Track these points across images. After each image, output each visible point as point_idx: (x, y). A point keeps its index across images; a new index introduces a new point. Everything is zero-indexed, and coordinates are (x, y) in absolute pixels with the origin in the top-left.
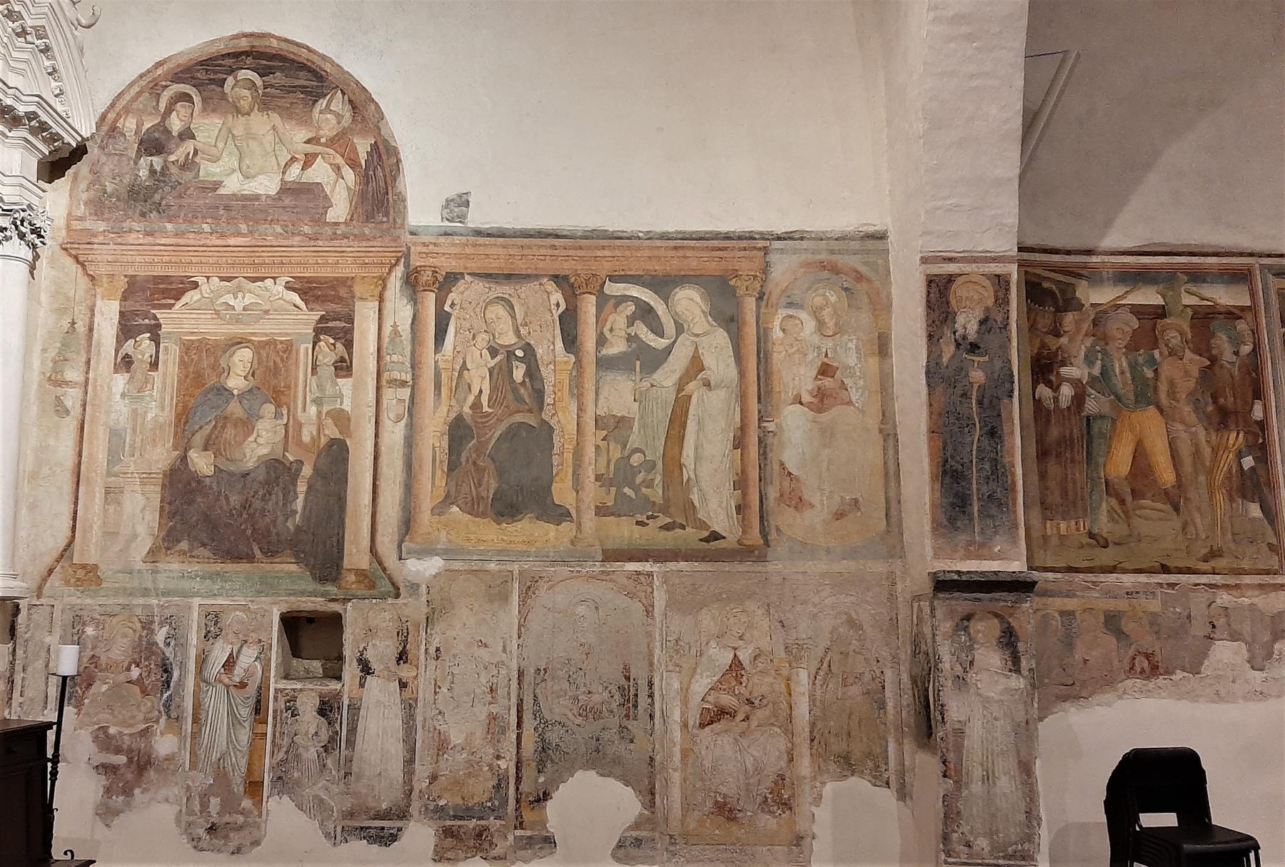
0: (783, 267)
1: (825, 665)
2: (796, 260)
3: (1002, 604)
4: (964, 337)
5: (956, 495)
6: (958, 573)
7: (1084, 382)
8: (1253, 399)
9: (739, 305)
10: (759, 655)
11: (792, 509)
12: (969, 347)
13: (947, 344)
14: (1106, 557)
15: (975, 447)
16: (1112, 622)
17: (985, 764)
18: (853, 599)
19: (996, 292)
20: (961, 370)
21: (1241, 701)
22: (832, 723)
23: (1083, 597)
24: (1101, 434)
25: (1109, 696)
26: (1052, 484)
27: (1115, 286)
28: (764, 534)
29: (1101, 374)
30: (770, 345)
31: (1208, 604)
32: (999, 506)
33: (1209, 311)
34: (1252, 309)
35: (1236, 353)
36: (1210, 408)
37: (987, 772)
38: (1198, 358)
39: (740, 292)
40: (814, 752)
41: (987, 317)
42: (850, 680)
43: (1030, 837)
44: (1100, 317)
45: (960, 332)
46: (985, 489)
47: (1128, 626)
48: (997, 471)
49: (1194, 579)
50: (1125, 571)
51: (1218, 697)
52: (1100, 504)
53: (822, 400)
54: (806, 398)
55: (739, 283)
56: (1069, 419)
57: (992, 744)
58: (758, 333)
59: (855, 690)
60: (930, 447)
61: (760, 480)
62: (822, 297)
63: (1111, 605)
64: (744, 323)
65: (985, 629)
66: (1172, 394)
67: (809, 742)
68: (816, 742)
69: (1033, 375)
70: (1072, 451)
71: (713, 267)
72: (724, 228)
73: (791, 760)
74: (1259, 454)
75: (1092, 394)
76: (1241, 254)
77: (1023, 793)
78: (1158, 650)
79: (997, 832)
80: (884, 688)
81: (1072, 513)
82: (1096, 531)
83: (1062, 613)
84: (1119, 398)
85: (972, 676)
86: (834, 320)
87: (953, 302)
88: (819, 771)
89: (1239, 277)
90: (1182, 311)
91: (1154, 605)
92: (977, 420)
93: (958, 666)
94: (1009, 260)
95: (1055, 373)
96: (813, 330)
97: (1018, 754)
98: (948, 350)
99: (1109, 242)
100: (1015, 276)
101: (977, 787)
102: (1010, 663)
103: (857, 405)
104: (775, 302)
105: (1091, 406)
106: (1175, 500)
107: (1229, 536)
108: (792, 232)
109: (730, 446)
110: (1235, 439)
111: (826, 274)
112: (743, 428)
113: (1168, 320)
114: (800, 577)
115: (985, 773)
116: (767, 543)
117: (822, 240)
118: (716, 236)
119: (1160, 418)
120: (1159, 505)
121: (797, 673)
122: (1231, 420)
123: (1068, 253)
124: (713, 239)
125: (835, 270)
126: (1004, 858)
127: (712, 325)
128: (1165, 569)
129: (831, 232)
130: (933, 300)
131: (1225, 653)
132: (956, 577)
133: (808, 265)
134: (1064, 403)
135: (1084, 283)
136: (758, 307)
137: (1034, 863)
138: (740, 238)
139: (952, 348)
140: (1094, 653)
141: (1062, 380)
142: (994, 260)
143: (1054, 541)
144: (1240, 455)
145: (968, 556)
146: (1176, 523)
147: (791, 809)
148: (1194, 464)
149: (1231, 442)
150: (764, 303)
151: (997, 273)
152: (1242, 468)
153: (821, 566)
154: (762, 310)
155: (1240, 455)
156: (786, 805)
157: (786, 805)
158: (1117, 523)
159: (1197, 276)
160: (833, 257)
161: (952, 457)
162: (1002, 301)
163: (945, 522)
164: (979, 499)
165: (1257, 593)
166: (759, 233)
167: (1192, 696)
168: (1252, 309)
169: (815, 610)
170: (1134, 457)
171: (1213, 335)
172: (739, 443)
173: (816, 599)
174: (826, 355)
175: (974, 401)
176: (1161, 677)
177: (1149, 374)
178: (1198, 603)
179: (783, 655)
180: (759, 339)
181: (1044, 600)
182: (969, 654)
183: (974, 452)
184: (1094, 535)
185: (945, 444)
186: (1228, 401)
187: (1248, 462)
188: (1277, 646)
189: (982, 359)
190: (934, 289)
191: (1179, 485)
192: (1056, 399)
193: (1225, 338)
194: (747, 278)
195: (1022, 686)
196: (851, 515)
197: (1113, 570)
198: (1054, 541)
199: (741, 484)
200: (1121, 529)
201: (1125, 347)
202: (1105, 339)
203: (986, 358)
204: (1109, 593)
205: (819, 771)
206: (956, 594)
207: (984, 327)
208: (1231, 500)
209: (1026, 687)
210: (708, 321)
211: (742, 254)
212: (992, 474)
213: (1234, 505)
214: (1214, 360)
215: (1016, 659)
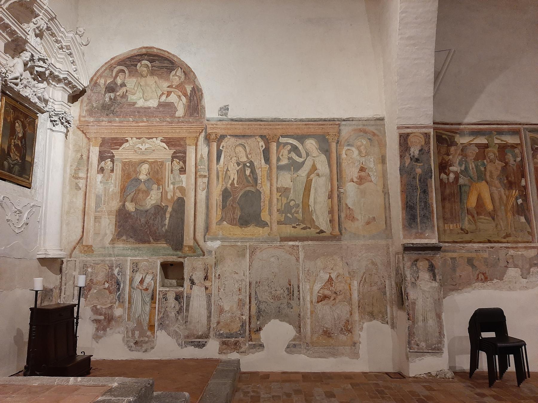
0: (346, 131)
1: (363, 279)
3: (429, 255)
4: (414, 156)
5: (412, 215)
6: (413, 244)
9: (329, 145)
14: (467, 237)
15: (418, 197)
16: (470, 261)
18: (374, 254)
19: (425, 139)
20: (413, 169)
21: (519, 290)
22: (366, 300)
24: (465, 191)
28: (340, 230)
29: (465, 169)
30: (341, 160)
33: (504, 145)
34: (521, 144)
35: (515, 161)
36: (505, 181)
38: (501, 163)
39: (330, 141)
40: (360, 311)
43: (440, 342)
44: (464, 148)
45: (412, 154)
47: (476, 263)
48: (427, 206)
50: (474, 243)
51: (510, 289)
53: (361, 180)
54: (355, 180)
55: (329, 137)
56: (453, 186)
58: (337, 156)
59: (375, 288)
61: (338, 210)
63: (470, 255)
65: (423, 265)
66: (491, 176)
68: (360, 307)
71: (320, 131)
72: (324, 117)
73: (351, 314)
76: (516, 124)
79: (428, 340)
81: (455, 221)
82: (463, 228)
83: (451, 258)
84: (471, 178)
85: (418, 282)
87: (409, 143)
89: (515, 132)
91: (486, 255)
93: (413, 278)
94: (430, 127)
98: (408, 161)
99: (466, 120)
100: (432, 133)
101: (420, 324)
102: (432, 277)
103: (374, 182)
105: (461, 181)
106: (493, 216)
107: (513, 229)
108: (349, 118)
109: (327, 198)
110: (515, 193)
111: (362, 133)
112: (332, 191)
113: (489, 149)
116: (341, 234)
118: (321, 120)
120: (487, 218)
123: (452, 124)
125: (365, 132)
127: (320, 153)
128: (490, 242)
129: (363, 118)
131: (513, 272)
133: (355, 130)
134: (451, 180)
135: (458, 135)
136: (337, 146)
138: (329, 121)
139: (409, 160)
142: (424, 127)
143: (448, 232)
144: (517, 199)
145: (416, 238)
146: (494, 224)
147: (351, 332)
149: (513, 194)
155: (517, 199)
156: (350, 331)
157: (350, 331)
158: (471, 224)
159: (500, 132)
160: (365, 127)
162: (427, 143)
163: (407, 225)
164: (420, 216)
165: (524, 250)
166: (336, 119)
167: (500, 288)
169: (359, 259)
172: (330, 197)
173: (360, 255)
175: (417, 180)
177: (483, 169)
178: (502, 254)
179: (348, 275)
183: (418, 199)
186: (512, 179)
187: (520, 201)
188: (532, 269)
189: (420, 164)
191: (494, 210)
192: (448, 179)
193: (510, 155)
194: (332, 135)
195: (437, 286)
197: (470, 242)
198: (448, 232)
199: (331, 212)
202: (466, 156)
204: (468, 251)
205: (362, 318)
206: (412, 252)
207: (421, 152)
208: (514, 215)
209: (438, 286)
211: (331, 126)
214: (507, 163)
215: (434, 276)
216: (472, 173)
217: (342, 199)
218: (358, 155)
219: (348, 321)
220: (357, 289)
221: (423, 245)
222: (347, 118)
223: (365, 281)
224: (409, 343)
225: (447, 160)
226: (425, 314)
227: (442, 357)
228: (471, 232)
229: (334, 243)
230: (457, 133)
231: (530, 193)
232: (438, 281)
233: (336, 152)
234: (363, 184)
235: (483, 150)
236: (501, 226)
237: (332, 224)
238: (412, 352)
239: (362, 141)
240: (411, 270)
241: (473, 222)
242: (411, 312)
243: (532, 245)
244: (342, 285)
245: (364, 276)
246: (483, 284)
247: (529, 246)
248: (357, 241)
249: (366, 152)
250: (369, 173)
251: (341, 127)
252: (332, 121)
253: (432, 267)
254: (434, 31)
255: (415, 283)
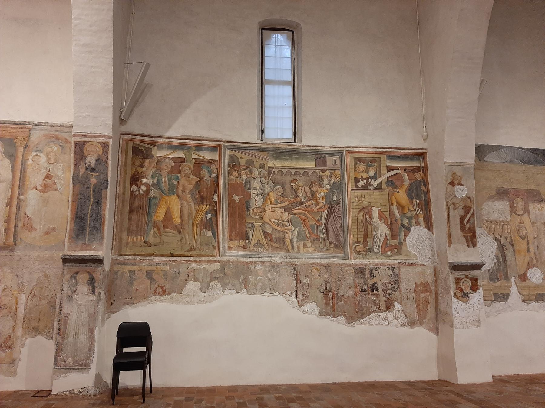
0: (36, 136)
1: (33, 292)
2: (42, 133)
3: (90, 268)
4: (89, 166)
5: (80, 226)
6: (70, 256)
7: (150, 185)
8: (214, 193)
9: (16, 151)
10: (6, 288)
11: (28, 231)
12: (91, 169)
13: (82, 168)
14: (150, 250)
15: (90, 207)
16: (149, 275)
17: (75, 329)
18: (48, 266)
19: (103, 149)
20: (87, 178)
21: (196, 304)
22: (33, 315)
23: (139, 265)
24: (154, 204)
25: (146, 303)
26: (133, 223)
27: (167, 150)
28: (15, 240)
29: (157, 182)
30: (26, 166)
31: (187, 268)
32: (97, 230)
33: (201, 161)
34: (218, 161)
35: (210, 177)
36: (197, 196)
37: (76, 333)
38: (195, 177)
39: (17, 145)
40: (24, 326)
41: (99, 158)
42: (43, 298)
43: (89, 358)
44: (160, 161)
45: (88, 163)
46: (92, 224)
47: (155, 276)
48: (99, 218)
49: (183, 258)
50: (156, 256)
51: (187, 303)
52: (151, 230)
53: (45, 188)
54: (39, 187)
55: (17, 141)
56: (143, 198)
57: (79, 322)
58: (22, 161)
59: (44, 302)
60: (72, 207)
61: (16, 219)
62: (51, 148)
63: (149, 268)
64: (17, 157)
65: (83, 277)
66: (183, 190)
67: (22, 322)
68: (25, 323)
69: (131, 181)
70: (143, 210)
71: (8, 135)
72: (14, 120)
73: (14, 330)
74: (214, 213)
75: (153, 190)
76: (217, 141)
77: (89, 341)
78: (166, 286)
79: (76, 356)
80: (56, 301)
81: (139, 233)
82: (147, 240)
83: (130, 271)
84: (163, 192)
85: (75, 296)
86: (54, 158)
87: (85, 152)
88: (25, 334)
89: (215, 149)
90: (191, 161)
91: (166, 268)
92: (92, 197)
93: (70, 292)
94: (110, 137)
95: (139, 181)
96: (45, 161)
97: (89, 325)
98: (82, 170)
99: (168, 134)
100: (111, 143)
101: (71, 339)
102: (91, 290)
103: (59, 190)
104: (31, 149)
105: (152, 194)
106: (179, 230)
107: (199, 243)
108: (41, 123)
109: (5, 205)
110: (205, 207)
111: (53, 140)
112: (11, 198)
113: (186, 164)
114: (27, 257)
115: (75, 333)
116: (15, 244)
117: (53, 126)
118: (11, 122)
119: (178, 199)
120: (173, 231)
121: (21, 295)
122: (205, 201)
123: (152, 137)
124: (9, 124)
125: (57, 138)
126: (78, 366)
127: (4, 157)
128: (172, 255)
129: (57, 123)
130: (77, 151)
131: (192, 286)
132: (68, 257)
133: (46, 136)
134: (142, 192)
135: (156, 148)
136: (24, 151)
137: (90, 368)
138: (20, 124)
139: (84, 170)
140: (141, 286)
141: (142, 183)
142: (103, 137)
143: (131, 244)
144: (206, 214)
145: (81, 250)
146: (179, 238)
147: (11, 349)
148: (189, 216)
149: (204, 208)
150: (26, 150)
151: (103, 142)
152: (206, 217)
153: (37, 254)
154: (26, 152)
155: (206, 214)
156: (10, 347)
157: (10, 347)
158: (156, 237)
159: (199, 148)
160: (58, 133)
161: (81, 211)
162: (106, 153)
163: (74, 236)
164: (89, 228)
165: (206, 264)
166: (28, 122)
167: (177, 302)
168: (218, 161)
169: (32, 271)
170: (166, 213)
171: (202, 170)
172: (9, 204)
173: (33, 266)
174: (49, 171)
175: (91, 190)
176: (166, 295)
177: (175, 183)
178: (183, 268)
179: (16, 288)
180: (22, 164)
181: (123, 266)
182: (75, 287)
183: (90, 210)
184: (147, 242)
185: (78, 206)
186: (205, 194)
187: (209, 216)
188: (211, 283)
189: (96, 174)
190: (78, 147)
191: (181, 224)
192: (139, 191)
193: (206, 171)
194: (21, 139)
195: (94, 299)
196: (52, 233)
197: (152, 255)
198: (131, 244)
199: (7, 221)
200: (157, 240)
201: (168, 173)
202: (160, 169)
203: (98, 174)
204: (149, 264)
205: (25, 334)
206: (72, 264)
207: (97, 162)
208: (201, 229)
209: (96, 300)
210: (2, 156)
211: (21, 130)
212: (96, 218)
213: (202, 232)
214: (201, 179)
215: (93, 289)
216: (163, 187)
217: (22, 207)
218: (46, 162)
219: (10, 337)
220: (24, 303)
221: (81, 257)
222: (39, 123)
223: (35, 294)
224: (56, 359)
225: (140, 172)
226: (78, 328)
227: (88, 373)
228: (154, 245)
229: (6, 253)
230: (155, 145)
231: (221, 208)
232: (96, 294)
233: (23, 157)
234: (48, 192)
235: (179, 164)
236: (186, 239)
237: (7, 234)
238: (58, 369)
239: (53, 147)
240: (69, 283)
241: (159, 235)
242: (62, 326)
243: (216, 259)
244: (8, 298)
245: (34, 290)
246: (160, 297)
247: (212, 260)
248: (32, 252)
249: (55, 159)
250: (56, 181)
251: (32, 131)
252: (23, 124)
253: (92, 281)
254: (111, 41)
255: (71, 297)
